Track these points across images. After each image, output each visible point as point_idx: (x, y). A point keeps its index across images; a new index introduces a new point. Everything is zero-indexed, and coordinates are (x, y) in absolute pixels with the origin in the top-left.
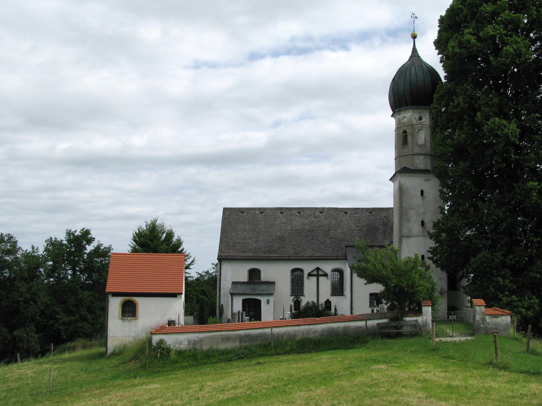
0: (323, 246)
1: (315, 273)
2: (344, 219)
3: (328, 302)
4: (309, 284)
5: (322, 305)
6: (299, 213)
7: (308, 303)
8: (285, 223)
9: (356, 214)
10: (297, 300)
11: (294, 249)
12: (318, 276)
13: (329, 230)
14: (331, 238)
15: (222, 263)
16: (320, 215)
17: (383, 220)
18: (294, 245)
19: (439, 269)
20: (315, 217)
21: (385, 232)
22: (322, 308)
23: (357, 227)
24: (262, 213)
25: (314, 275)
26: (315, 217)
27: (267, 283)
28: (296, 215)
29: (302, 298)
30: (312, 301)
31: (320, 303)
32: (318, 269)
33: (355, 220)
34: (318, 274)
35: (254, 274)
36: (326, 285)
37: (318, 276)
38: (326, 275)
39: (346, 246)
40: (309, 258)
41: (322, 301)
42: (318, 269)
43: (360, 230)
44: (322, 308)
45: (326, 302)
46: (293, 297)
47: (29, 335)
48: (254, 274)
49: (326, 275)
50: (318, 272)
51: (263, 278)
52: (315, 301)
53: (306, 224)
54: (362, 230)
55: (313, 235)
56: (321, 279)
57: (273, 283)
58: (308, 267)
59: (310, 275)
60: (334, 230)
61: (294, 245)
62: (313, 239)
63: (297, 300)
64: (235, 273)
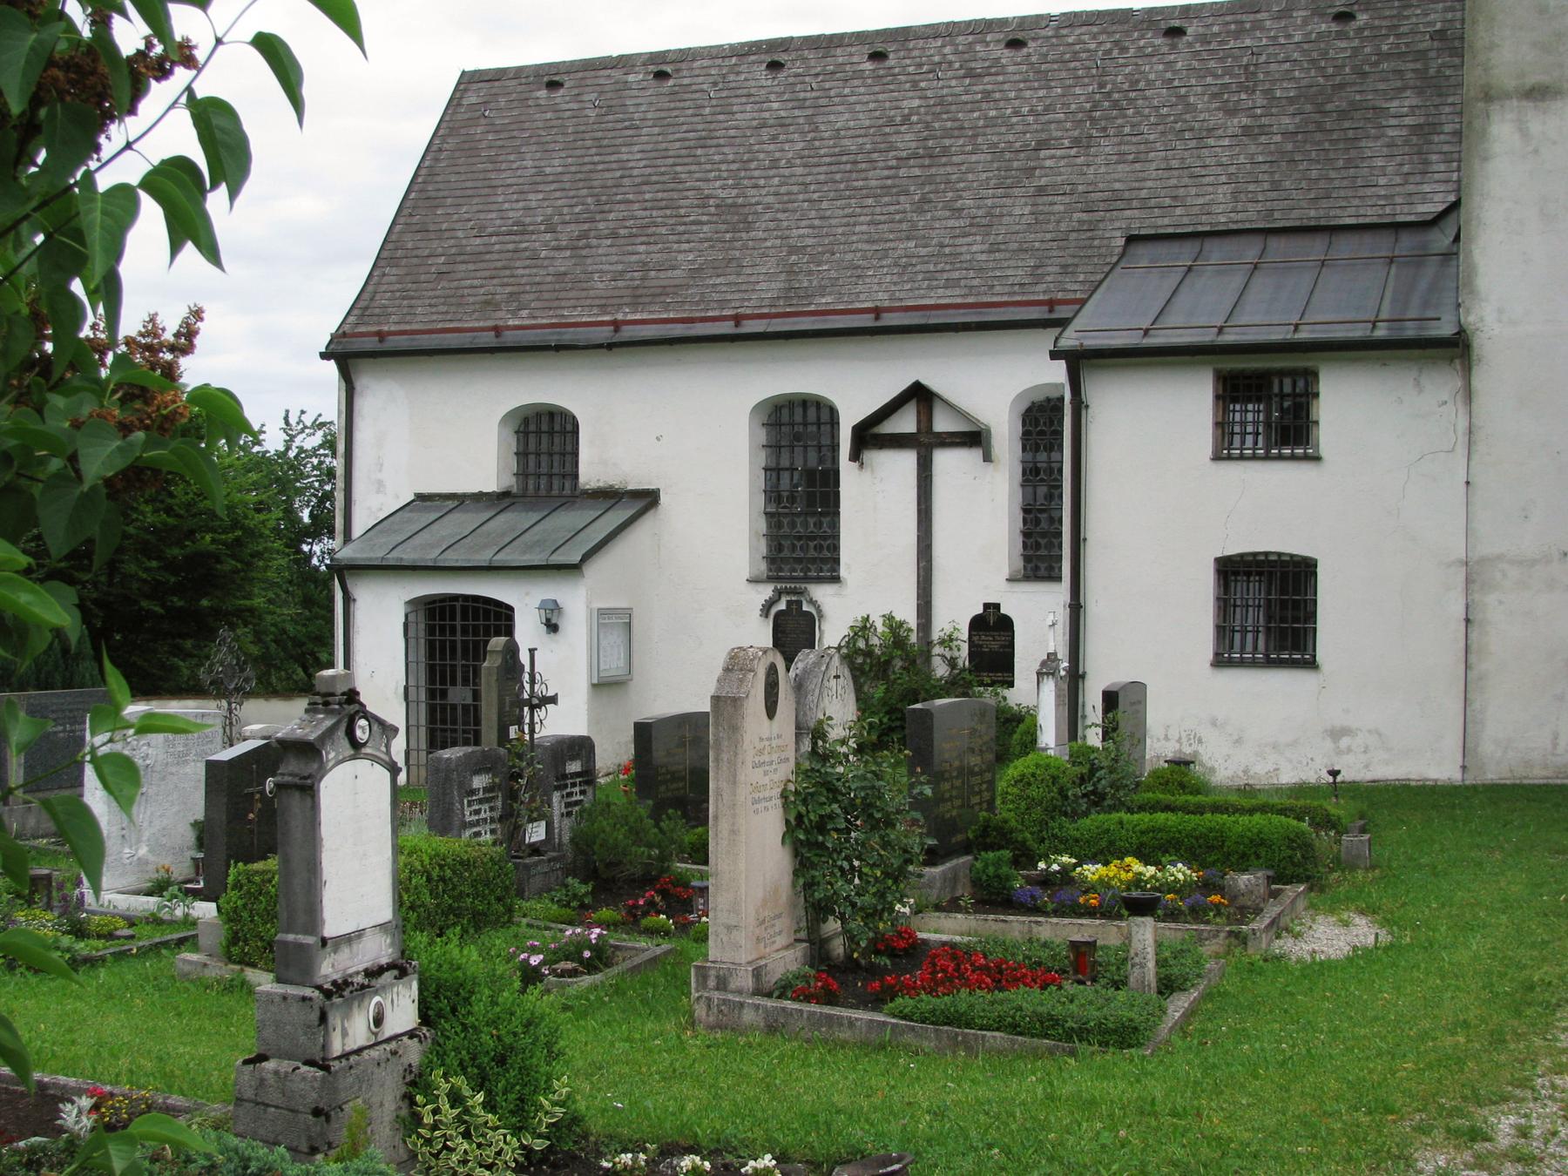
0: (976, 247)
1: (906, 423)
2: (1153, 70)
3: (993, 628)
4: (874, 496)
5: (948, 641)
6: (878, 56)
7: (864, 628)
8: (782, 124)
9: (1237, 34)
10: (794, 606)
11: (791, 272)
12: (925, 444)
13: (1042, 145)
14: (1041, 191)
15: (363, 382)
16: (1007, 55)
17: (1422, 55)
18: (793, 250)
19: (980, 610)
20: (971, 74)
21: (1425, 131)
22: (952, 663)
23: (1231, 112)
24: (661, 75)
25: (898, 442)
26: (971, 74)
27: (609, 496)
28: (859, 75)
29: (822, 594)
30: (889, 619)
31: (936, 635)
32: (920, 395)
33: (1228, 71)
34: (919, 427)
35: (545, 439)
36: (980, 503)
37: (925, 444)
38: (975, 438)
39: (1131, 240)
40: (866, 321)
41: (954, 614)
42: (920, 395)
43: (1247, 131)
44: (952, 663)
45: (977, 624)
46: (767, 591)
47: (1056, 492)
48: (545, 439)
49: (975, 438)
50: (926, 418)
51: (593, 469)
52: (907, 614)
53: (906, 119)
54: (1264, 130)
55: (930, 180)
56: (946, 461)
57: (648, 499)
58: (855, 386)
59: (869, 436)
60: (1076, 142)
61: (793, 250)
62: (923, 204)
63: (794, 606)
64: (433, 442)
